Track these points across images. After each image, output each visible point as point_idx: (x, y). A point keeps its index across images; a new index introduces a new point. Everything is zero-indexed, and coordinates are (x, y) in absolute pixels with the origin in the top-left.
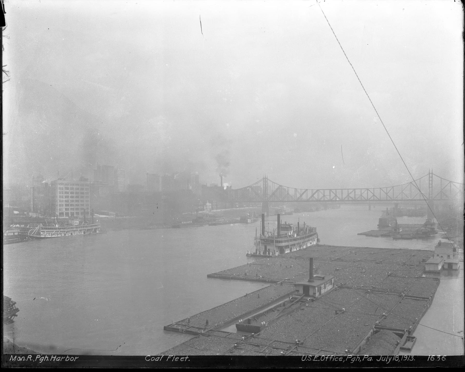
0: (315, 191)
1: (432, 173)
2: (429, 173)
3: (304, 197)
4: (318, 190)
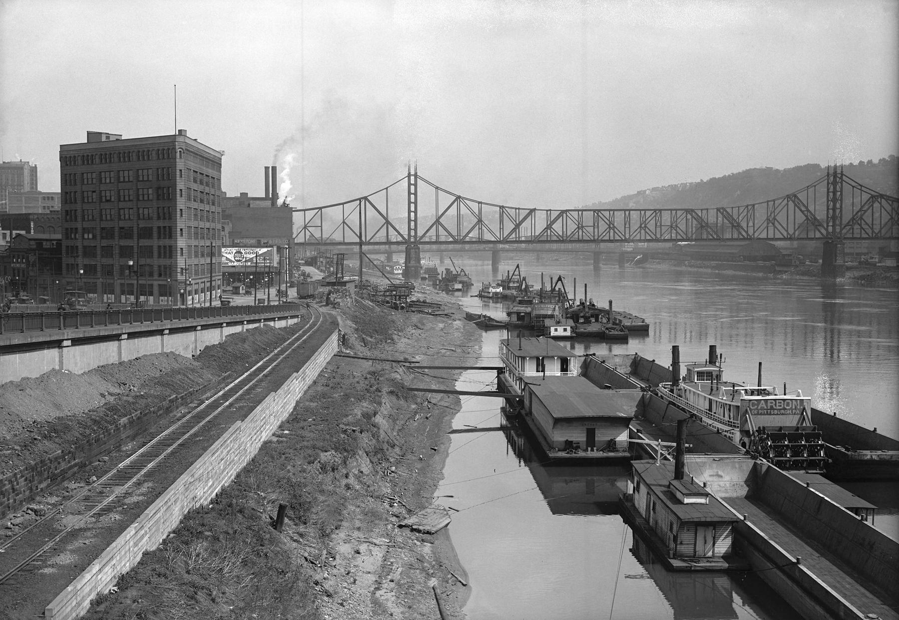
1: (842, 172)
2: (409, 175)
3: (526, 231)
4: (563, 212)
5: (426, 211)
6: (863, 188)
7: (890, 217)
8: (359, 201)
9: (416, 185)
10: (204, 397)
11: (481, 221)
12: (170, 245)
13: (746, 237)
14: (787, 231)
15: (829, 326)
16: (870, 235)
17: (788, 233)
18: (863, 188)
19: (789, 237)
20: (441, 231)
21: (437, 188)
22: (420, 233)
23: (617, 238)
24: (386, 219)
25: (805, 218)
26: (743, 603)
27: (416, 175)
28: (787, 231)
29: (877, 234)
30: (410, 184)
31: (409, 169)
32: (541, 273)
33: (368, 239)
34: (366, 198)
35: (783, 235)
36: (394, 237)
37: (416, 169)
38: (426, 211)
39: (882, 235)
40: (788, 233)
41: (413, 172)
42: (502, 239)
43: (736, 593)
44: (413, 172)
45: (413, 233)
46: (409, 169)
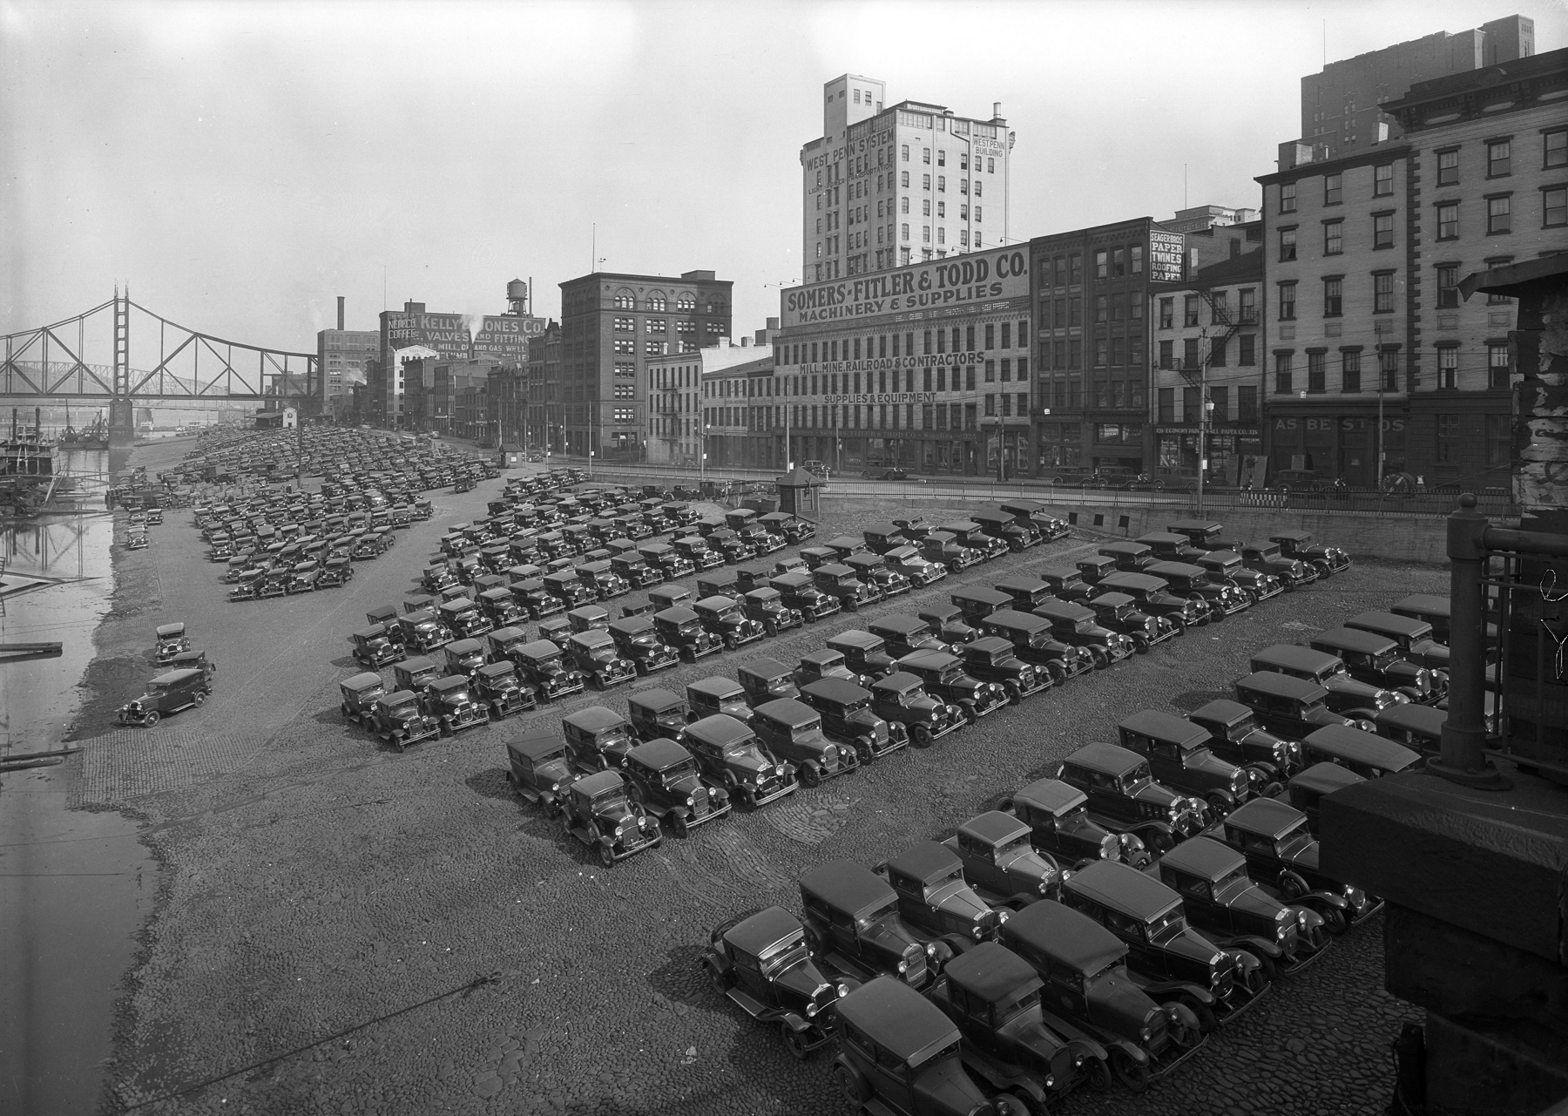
2: (116, 301)
5: (143, 359)
9: (126, 313)
12: (969, 401)
16: (112, 390)
20: (88, 379)
21: (163, 320)
22: (135, 380)
24: (229, 366)
27: (127, 301)
30: (117, 314)
31: (116, 292)
32: (11, 409)
35: (105, 387)
36: (90, 387)
37: (127, 293)
38: (143, 359)
41: (121, 296)
43: (1357, 785)
44: (121, 296)
45: (122, 381)
46: (116, 292)
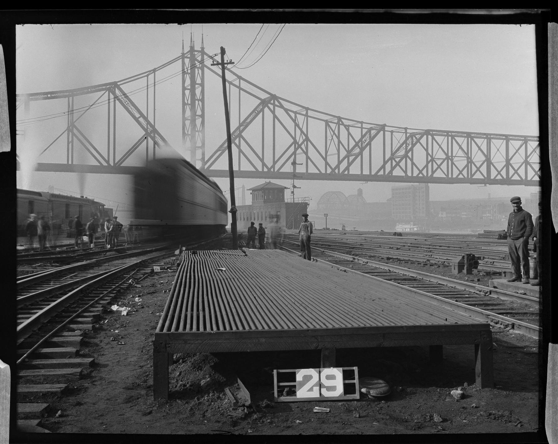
0: (356, 133)
1: (203, 48)
6: (151, 90)
7: (292, 141)
8: (146, 77)
10: (67, 290)
11: (155, 131)
13: (260, 169)
14: (262, 160)
15: (52, 232)
17: (264, 165)
18: (244, 85)
19: (329, 171)
23: (312, 170)
25: (292, 141)
26: (468, 385)
28: (262, 160)
29: (269, 169)
33: (454, 176)
34: (112, 87)
39: (341, 171)
40: (264, 165)
42: (112, 163)
